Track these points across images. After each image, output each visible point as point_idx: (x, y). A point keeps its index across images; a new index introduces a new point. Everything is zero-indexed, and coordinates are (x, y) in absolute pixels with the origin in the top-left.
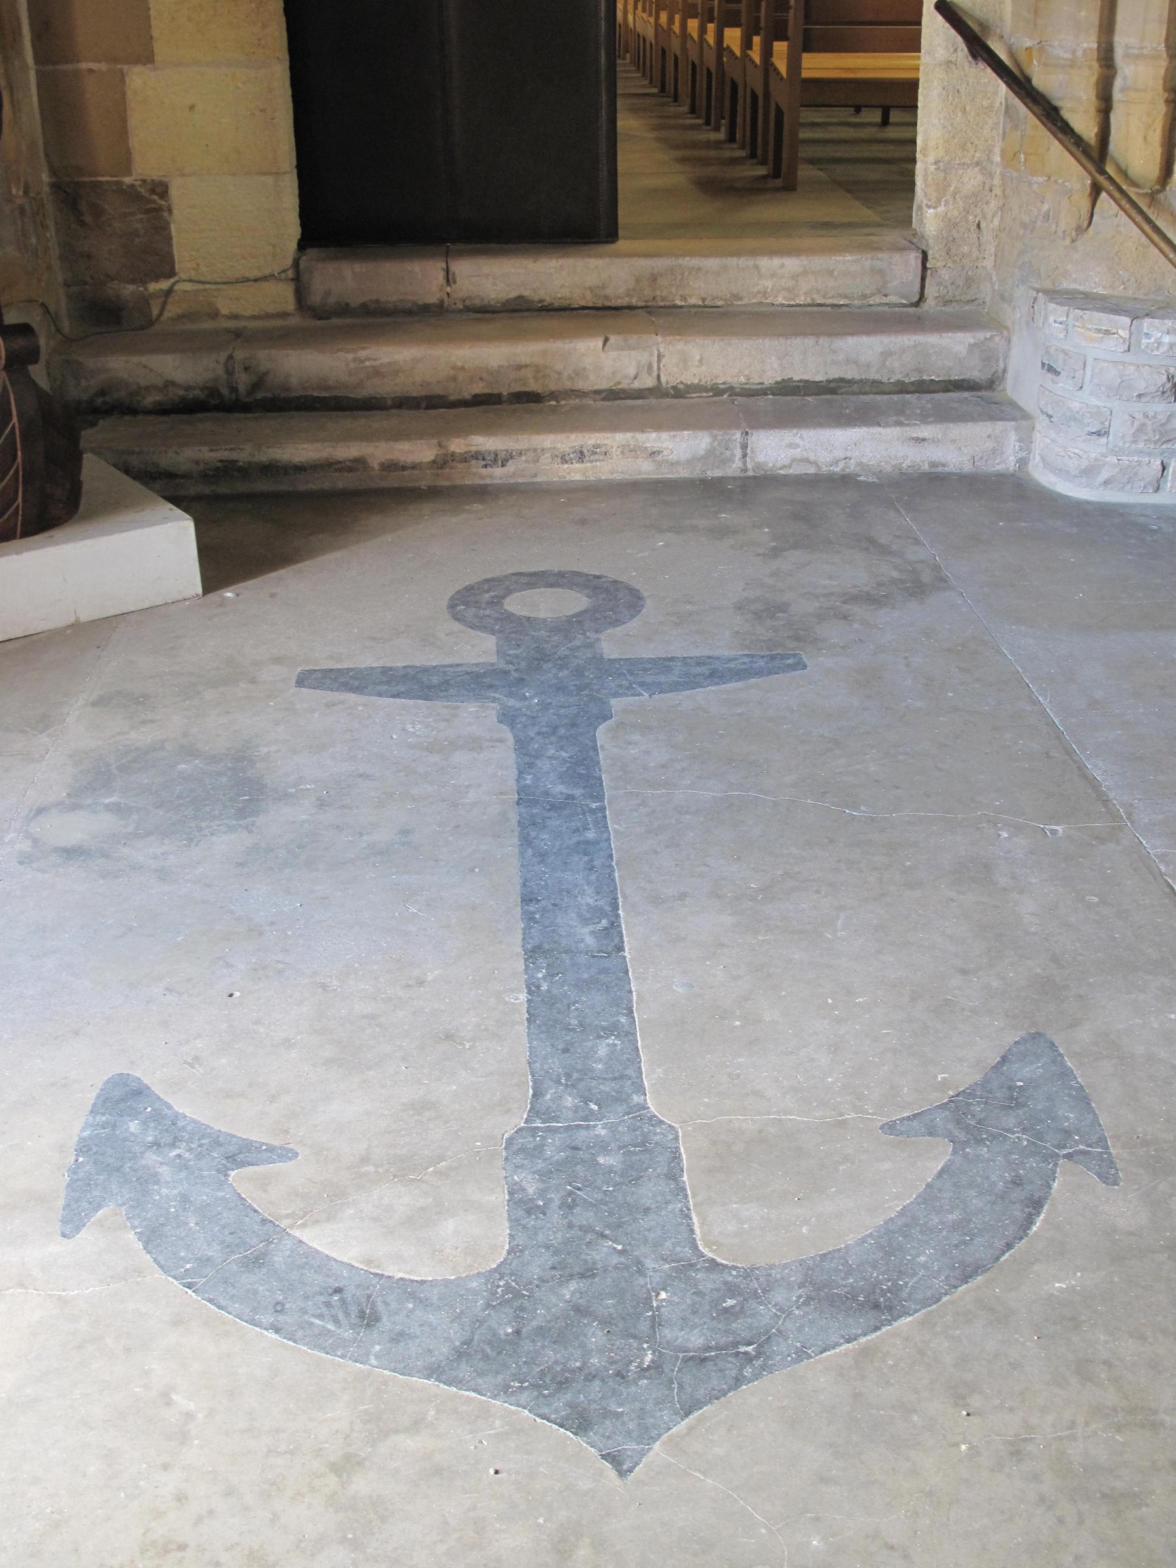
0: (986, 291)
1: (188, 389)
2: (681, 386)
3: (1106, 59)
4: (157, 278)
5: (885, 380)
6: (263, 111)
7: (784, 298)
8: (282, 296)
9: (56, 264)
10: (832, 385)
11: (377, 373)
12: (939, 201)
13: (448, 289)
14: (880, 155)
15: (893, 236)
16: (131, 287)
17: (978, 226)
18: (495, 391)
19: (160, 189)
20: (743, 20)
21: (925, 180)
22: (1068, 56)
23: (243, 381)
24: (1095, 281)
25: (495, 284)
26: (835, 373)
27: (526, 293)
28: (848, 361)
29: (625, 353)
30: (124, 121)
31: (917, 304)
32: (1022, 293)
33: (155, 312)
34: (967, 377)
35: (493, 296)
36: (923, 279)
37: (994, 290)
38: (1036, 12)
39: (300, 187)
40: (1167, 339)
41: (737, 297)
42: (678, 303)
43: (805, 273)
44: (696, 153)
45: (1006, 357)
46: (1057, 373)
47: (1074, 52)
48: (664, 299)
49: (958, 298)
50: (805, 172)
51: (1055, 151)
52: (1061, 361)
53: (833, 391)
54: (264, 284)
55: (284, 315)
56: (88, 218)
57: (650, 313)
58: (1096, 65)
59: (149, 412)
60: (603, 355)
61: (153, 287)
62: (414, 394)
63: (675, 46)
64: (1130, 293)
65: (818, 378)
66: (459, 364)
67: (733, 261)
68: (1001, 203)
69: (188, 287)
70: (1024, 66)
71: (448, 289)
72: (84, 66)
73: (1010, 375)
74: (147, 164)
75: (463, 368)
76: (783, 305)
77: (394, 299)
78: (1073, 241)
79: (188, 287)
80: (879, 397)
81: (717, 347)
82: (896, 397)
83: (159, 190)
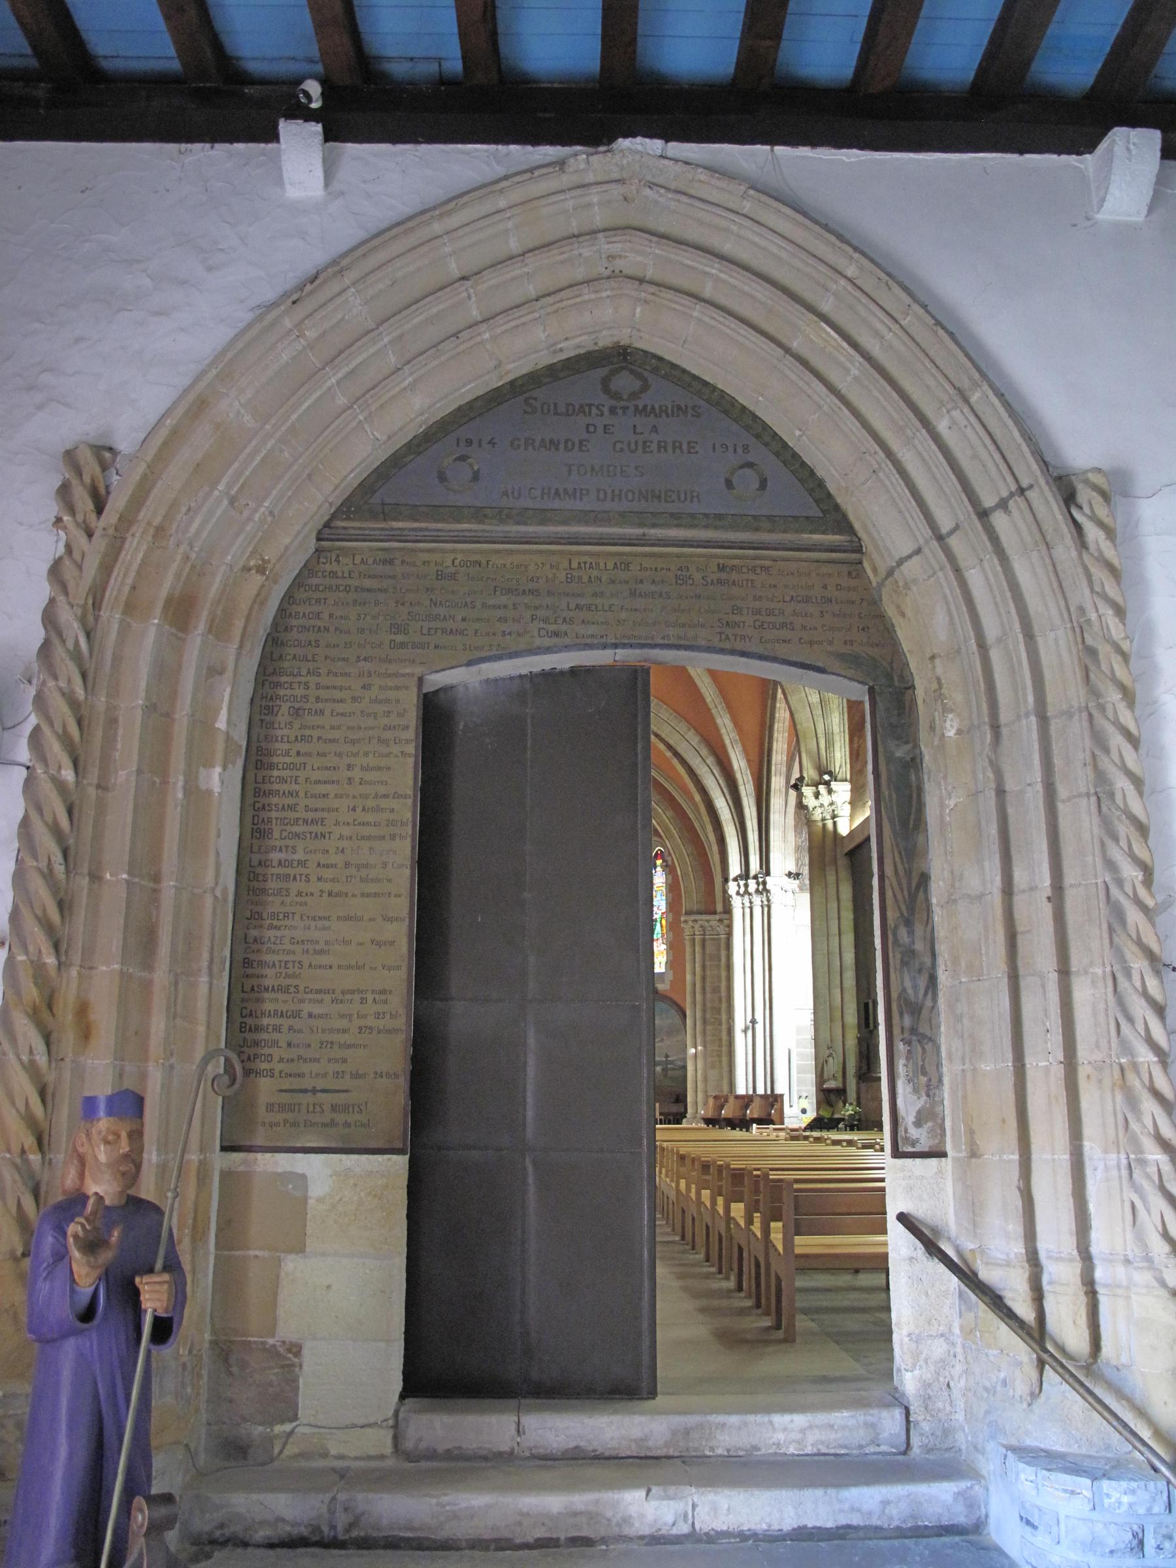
0: (962, 1440)
1: (295, 1524)
2: (712, 1533)
3: (1033, 1259)
4: (282, 1422)
5: (886, 1526)
6: (383, 1292)
7: (795, 1449)
8: (381, 1441)
9: (203, 1406)
10: (841, 1531)
11: (455, 1516)
12: (914, 1365)
13: (519, 1439)
14: (856, 1304)
15: (878, 1391)
16: (261, 1428)
17: (948, 1385)
18: (554, 1536)
19: (296, 1349)
20: (746, 1197)
21: (902, 1349)
22: (1003, 1257)
23: (342, 1520)
24: (1055, 1441)
25: (557, 1436)
26: (843, 1521)
27: (582, 1444)
28: (853, 1509)
29: (665, 1502)
30: (275, 1295)
31: (905, 1453)
32: (993, 1449)
33: (276, 1451)
34: (955, 1522)
35: (555, 1445)
36: (908, 1431)
37: (967, 1441)
38: (974, 1225)
39: (405, 1365)
40: (1125, 1499)
41: (756, 1448)
42: (708, 1453)
43: (811, 1427)
44: (715, 1303)
45: (986, 1505)
46: (1035, 1527)
47: (1008, 1254)
48: (696, 1450)
49: (938, 1446)
50: (802, 1323)
51: (1004, 1331)
52: (1037, 1516)
53: (843, 1537)
54: (368, 1430)
55: (382, 1457)
56: (234, 1369)
57: (684, 1462)
58: (1027, 1266)
59: (258, 1546)
60: (646, 1505)
61: (278, 1429)
62: (485, 1537)
63: (692, 1210)
64: (1084, 1451)
65: (830, 1525)
66: (525, 1510)
67: (751, 1418)
68: (965, 1367)
69: (307, 1430)
70: (970, 1262)
71: (519, 1439)
72: (251, 1253)
73: (992, 1521)
74: (288, 1329)
75: (528, 1514)
76: (793, 1455)
77: (474, 1446)
78: (1029, 1405)
79: (307, 1430)
80: (882, 1543)
81: (741, 1496)
82: (896, 1542)
83: (294, 1350)
